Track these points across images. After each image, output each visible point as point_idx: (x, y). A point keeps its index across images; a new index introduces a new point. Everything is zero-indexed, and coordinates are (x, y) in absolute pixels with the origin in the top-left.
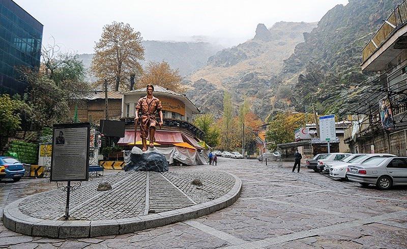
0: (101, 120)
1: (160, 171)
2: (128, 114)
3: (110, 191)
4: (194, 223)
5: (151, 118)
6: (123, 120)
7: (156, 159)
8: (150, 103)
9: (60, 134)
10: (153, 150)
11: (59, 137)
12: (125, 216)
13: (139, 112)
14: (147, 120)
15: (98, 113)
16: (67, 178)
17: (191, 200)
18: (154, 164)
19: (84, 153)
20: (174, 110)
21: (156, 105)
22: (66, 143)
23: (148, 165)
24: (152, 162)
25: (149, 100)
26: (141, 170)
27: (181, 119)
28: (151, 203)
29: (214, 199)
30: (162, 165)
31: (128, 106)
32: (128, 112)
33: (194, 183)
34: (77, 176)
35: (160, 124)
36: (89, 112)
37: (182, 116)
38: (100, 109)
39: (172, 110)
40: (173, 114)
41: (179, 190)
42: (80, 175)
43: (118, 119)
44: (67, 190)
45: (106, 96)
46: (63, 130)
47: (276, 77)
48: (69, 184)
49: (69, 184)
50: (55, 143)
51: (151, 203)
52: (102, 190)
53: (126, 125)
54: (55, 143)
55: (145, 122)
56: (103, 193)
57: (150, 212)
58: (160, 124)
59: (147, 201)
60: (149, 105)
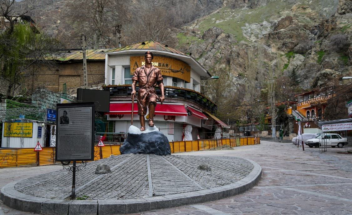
0: (78, 89)
1: (161, 154)
2: (113, 81)
3: (109, 174)
4: (201, 207)
5: (150, 91)
6: (106, 88)
7: (157, 140)
8: (149, 74)
9: (64, 114)
10: (153, 129)
11: (63, 117)
12: (130, 197)
13: (136, 83)
14: (146, 93)
15: (73, 80)
16: (72, 158)
17: (198, 185)
18: (154, 146)
19: (89, 133)
20: (177, 75)
21: (155, 76)
22: (71, 123)
23: (147, 147)
24: (152, 144)
25: (148, 70)
26: (140, 153)
27: (185, 86)
28: (154, 186)
29: (224, 185)
30: (164, 147)
31: (114, 70)
32: (113, 77)
33: (201, 168)
34: (82, 156)
35: (162, 98)
36: (61, 78)
37: (186, 82)
38: (76, 74)
39: (172, 74)
40: (175, 80)
41: (185, 175)
42: (85, 154)
43: (100, 88)
44: (72, 170)
45: (84, 57)
46: (67, 110)
47: (327, 21)
48: (74, 165)
49: (74, 165)
50: (59, 122)
51: (154, 186)
52: (100, 173)
53: (111, 95)
54: (59, 122)
55: (144, 96)
56: (102, 176)
57: (154, 195)
58: (162, 98)
59: (150, 185)
60: (148, 76)
